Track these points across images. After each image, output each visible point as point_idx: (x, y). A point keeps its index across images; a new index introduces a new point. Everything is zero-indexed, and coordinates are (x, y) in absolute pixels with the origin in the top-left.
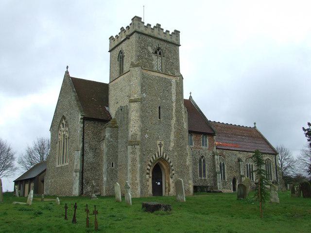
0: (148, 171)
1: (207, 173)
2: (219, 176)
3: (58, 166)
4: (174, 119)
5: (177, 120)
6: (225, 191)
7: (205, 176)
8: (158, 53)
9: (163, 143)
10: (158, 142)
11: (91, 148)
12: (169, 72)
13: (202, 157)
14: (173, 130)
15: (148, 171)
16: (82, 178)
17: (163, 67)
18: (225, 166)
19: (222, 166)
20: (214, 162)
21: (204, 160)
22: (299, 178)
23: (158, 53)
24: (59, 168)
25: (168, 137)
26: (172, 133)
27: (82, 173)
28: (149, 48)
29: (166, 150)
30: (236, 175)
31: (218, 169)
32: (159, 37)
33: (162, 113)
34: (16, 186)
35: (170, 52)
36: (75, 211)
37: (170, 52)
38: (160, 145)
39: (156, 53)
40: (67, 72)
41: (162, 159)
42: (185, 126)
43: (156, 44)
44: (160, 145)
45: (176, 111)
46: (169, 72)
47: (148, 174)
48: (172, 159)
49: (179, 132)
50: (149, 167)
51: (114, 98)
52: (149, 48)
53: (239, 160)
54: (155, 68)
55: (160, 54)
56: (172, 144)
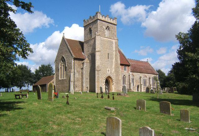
0: (103, 82)
1: (126, 83)
2: (132, 85)
3: (60, 79)
4: (114, 59)
5: (116, 60)
6: (135, 91)
7: (125, 84)
8: (108, 29)
9: (109, 69)
10: (108, 69)
11: (77, 72)
12: (112, 38)
13: (124, 75)
14: (114, 64)
15: (103, 82)
16: (74, 85)
17: (110, 35)
18: (134, 80)
19: (133, 79)
20: (129, 78)
21: (125, 77)
22: (141, 24)
23: (108, 29)
24: (61, 80)
25: (112, 67)
26: (113, 65)
27: (74, 82)
28: (104, 27)
29: (111, 73)
30: (139, 84)
31: (131, 82)
32: (108, 21)
33: (109, 56)
34: (174, 92)
35: (112, 28)
36: (68, 99)
37: (112, 28)
38: (108, 71)
39: (107, 29)
40: (64, 36)
41: (109, 77)
42: (119, 62)
43: (107, 24)
44: (108, 71)
45: (115, 56)
46: (112, 38)
47: (103, 83)
48: (114, 77)
49: (116, 64)
50: (104, 80)
51: (136, 74)
52: (104, 27)
53: (140, 78)
54: (106, 36)
55: (108, 29)
56: (113, 70)
